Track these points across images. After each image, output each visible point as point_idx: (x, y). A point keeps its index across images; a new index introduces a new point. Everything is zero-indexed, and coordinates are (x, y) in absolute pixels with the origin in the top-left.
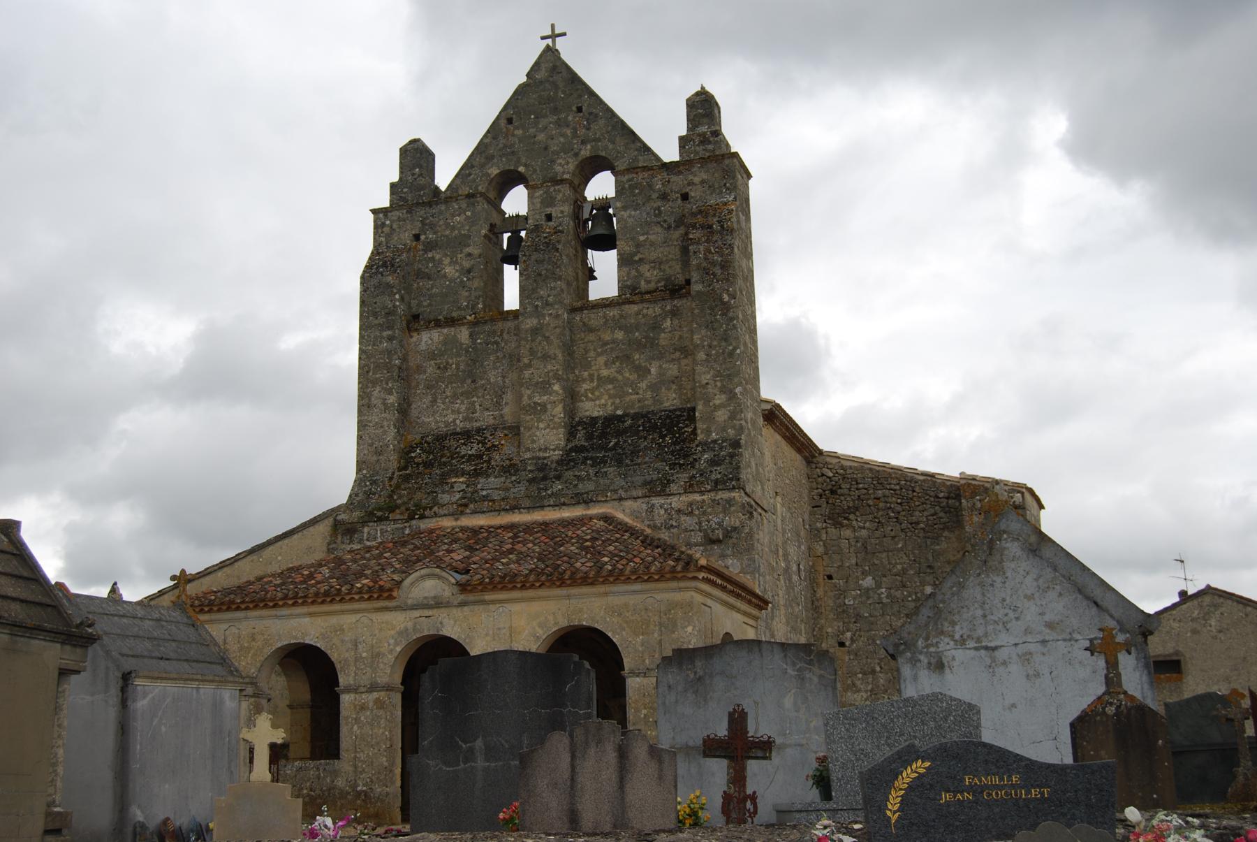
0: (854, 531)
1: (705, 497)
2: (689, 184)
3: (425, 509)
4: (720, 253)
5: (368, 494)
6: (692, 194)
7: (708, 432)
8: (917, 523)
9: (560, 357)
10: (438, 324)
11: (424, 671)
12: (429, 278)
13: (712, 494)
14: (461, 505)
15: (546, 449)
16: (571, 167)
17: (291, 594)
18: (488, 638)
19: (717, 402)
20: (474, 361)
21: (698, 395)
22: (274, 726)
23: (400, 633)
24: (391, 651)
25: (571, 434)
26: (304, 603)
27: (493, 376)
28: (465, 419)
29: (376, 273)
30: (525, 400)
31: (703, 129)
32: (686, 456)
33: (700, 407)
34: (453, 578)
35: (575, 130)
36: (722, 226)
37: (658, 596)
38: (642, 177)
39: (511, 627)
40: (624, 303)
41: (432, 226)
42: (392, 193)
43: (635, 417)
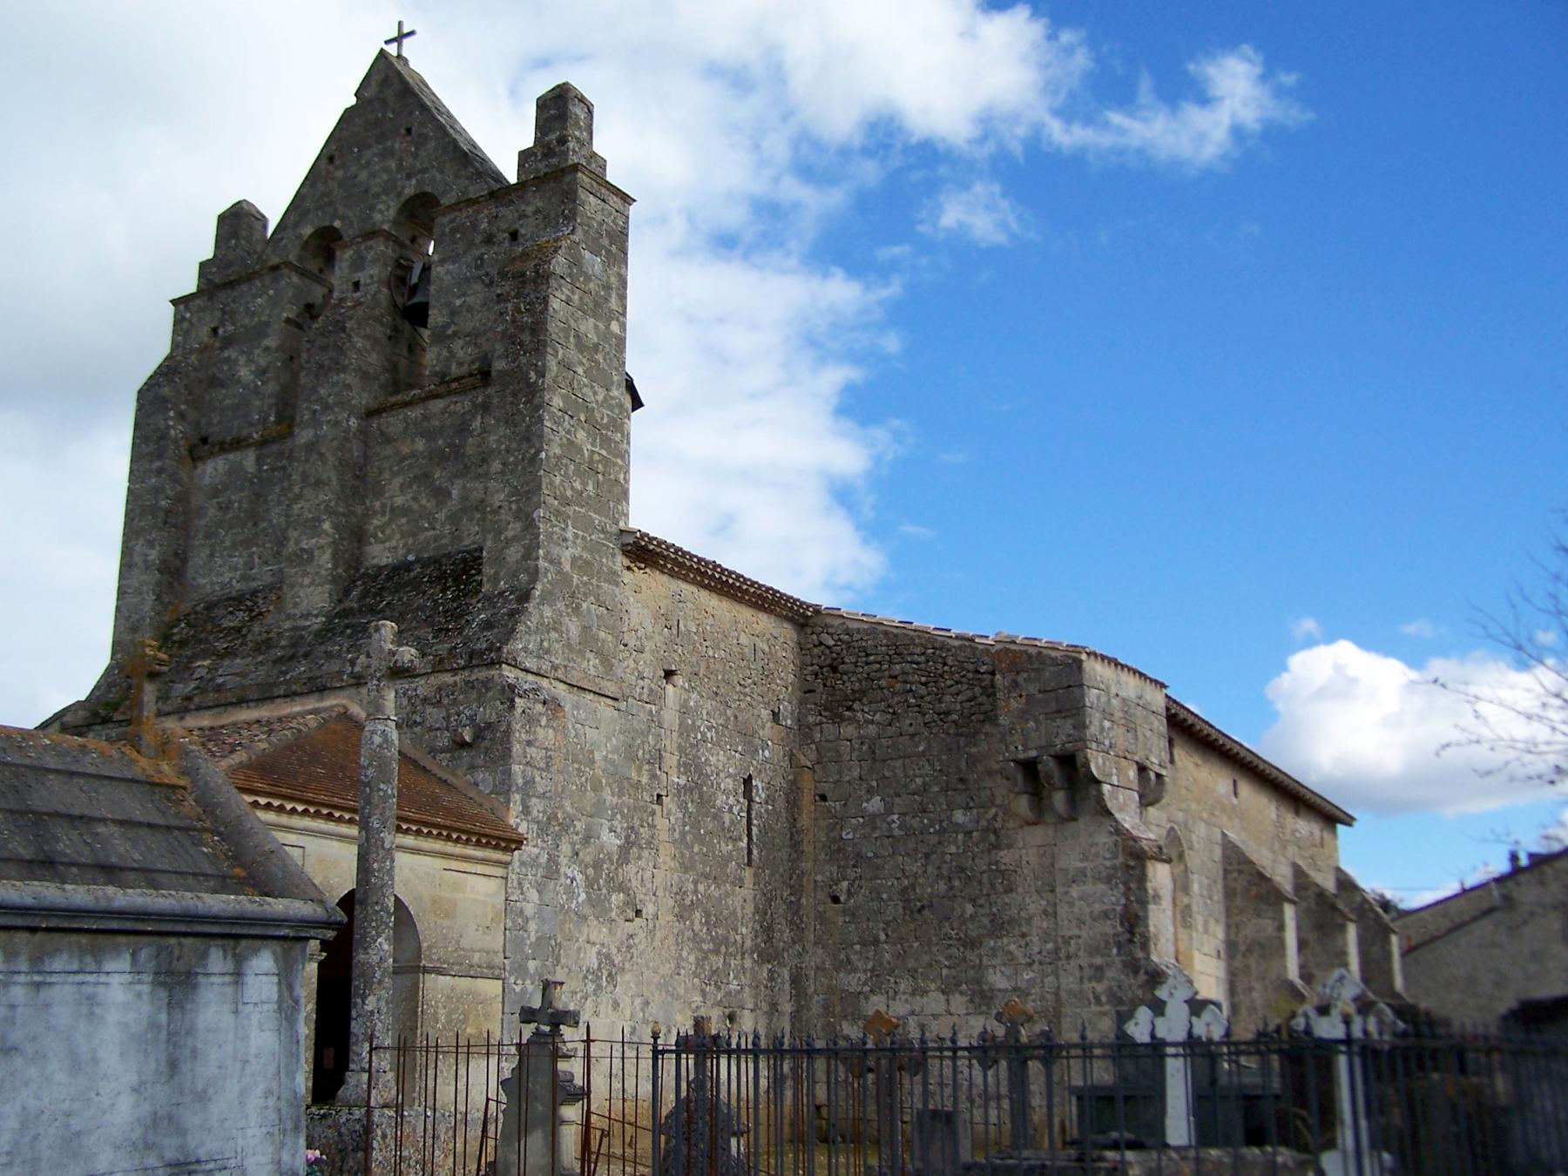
0: (859, 727)
1: (457, 678)
2: (520, 218)
6: (523, 231)
7: (495, 579)
8: (948, 713)
12: (223, 386)
13: (467, 673)
16: (392, 213)
19: (510, 534)
28: (245, 578)
31: (553, 137)
33: (489, 543)
43: (425, 564)
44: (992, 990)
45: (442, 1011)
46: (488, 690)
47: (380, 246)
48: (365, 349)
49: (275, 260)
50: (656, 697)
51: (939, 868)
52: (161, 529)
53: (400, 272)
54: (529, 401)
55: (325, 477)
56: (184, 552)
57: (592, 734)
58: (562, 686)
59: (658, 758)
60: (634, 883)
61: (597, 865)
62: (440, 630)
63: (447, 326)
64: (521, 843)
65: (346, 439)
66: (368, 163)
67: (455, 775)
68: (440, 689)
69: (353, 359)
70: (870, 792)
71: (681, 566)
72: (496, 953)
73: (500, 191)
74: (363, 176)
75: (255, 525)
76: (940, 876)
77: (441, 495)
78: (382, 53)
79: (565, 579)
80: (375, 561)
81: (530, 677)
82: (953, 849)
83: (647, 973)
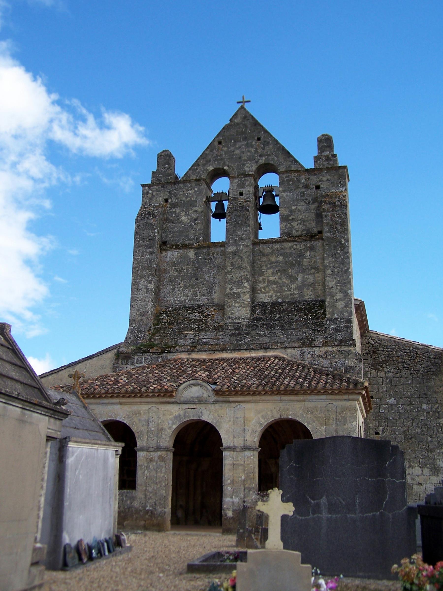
1: (334, 349)
2: (320, 181)
3: (171, 348)
4: (340, 217)
5: (137, 338)
6: (322, 186)
7: (332, 313)
8: (419, 371)
10: (177, 247)
11: (283, 448)
13: (338, 348)
14: (192, 347)
15: (239, 318)
16: (254, 168)
17: (110, 391)
18: (230, 423)
19: (338, 298)
20: (197, 268)
21: (327, 293)
22: (285, 499)
23: (176, 417)
24: (170, 428)
25: (253, 311)
26: (117, 397)
27: (208, 277)
28: (191, 300)
29: (144, 218)
30: (228, 291)
32: (321, 326)
33: (328, 300)
34: (210, 388)
35: (256, 149)
36: (341, 203)
37: (336, 403)
38: (293, 176)
39: (245, 417)
40: (283, 242)
41: (176, 195)
42: (153, 177)
43: (289, 303)
44: (438, 467)
46: (349, 355)
51: (417, 424)
70: (391, 396)
76: (418, 427)
80: (261, 300)
82: (423, 418)
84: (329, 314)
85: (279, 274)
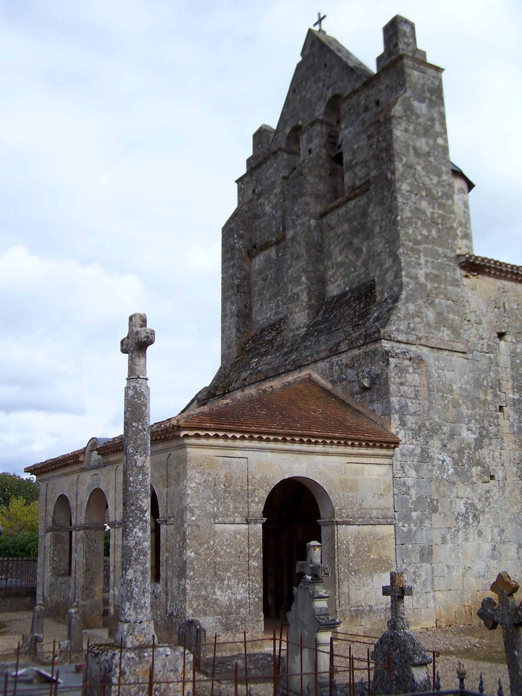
1: (360, 351)
6: (381, 100)
7: (382, 292)
9: (305, 255)
13: (365, 347)
16: (323, 110)
19: (387, 266)
28: (276, 313)
45: (352, 546)
46: (375, 356)
47: (318, 128)
48: (314, 182)
49: (275, 148)
50: (491, 349)
52: (236, 295)
53: (331, 140)
54: (389, 190)
55: (300, 254)
56: (250, 305)
57: (449, 375)
58: (425, 349)
59: (497, 384)
60: (487, 460)
61: (460, 451)
62: (356, 325)
63: (352, 160)
64: (398, 443)
65: (309, 231)
66: (310, 88)
67: (363, 406)
68: (353, 359)
69: (308, 188)
71: (501, 271)
72: (388, 509)
73: (370, 81)
74: (308, 95)
75: (278, 285)
77: (358, 251)
78: (310, 31)
79: (422, 287)
80: (331, 294)
81: (403, 346)
83: (501, 513)
84: (379, 294)
85: (345, 250)
